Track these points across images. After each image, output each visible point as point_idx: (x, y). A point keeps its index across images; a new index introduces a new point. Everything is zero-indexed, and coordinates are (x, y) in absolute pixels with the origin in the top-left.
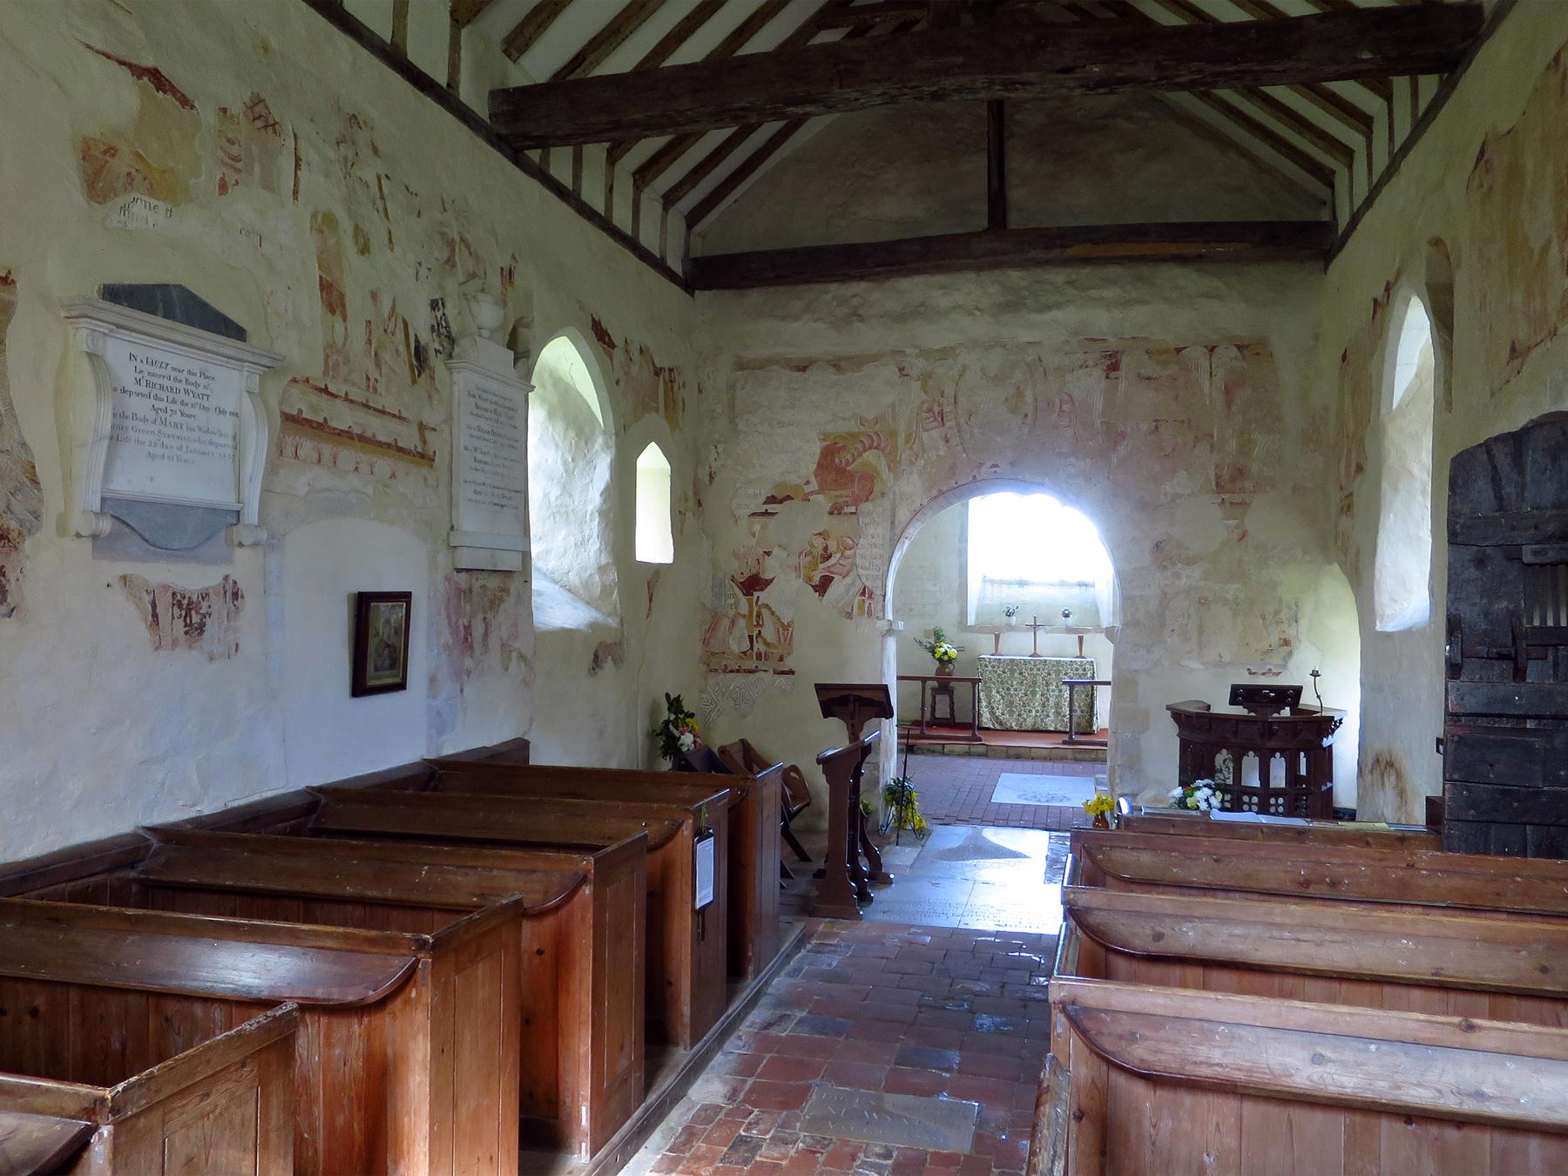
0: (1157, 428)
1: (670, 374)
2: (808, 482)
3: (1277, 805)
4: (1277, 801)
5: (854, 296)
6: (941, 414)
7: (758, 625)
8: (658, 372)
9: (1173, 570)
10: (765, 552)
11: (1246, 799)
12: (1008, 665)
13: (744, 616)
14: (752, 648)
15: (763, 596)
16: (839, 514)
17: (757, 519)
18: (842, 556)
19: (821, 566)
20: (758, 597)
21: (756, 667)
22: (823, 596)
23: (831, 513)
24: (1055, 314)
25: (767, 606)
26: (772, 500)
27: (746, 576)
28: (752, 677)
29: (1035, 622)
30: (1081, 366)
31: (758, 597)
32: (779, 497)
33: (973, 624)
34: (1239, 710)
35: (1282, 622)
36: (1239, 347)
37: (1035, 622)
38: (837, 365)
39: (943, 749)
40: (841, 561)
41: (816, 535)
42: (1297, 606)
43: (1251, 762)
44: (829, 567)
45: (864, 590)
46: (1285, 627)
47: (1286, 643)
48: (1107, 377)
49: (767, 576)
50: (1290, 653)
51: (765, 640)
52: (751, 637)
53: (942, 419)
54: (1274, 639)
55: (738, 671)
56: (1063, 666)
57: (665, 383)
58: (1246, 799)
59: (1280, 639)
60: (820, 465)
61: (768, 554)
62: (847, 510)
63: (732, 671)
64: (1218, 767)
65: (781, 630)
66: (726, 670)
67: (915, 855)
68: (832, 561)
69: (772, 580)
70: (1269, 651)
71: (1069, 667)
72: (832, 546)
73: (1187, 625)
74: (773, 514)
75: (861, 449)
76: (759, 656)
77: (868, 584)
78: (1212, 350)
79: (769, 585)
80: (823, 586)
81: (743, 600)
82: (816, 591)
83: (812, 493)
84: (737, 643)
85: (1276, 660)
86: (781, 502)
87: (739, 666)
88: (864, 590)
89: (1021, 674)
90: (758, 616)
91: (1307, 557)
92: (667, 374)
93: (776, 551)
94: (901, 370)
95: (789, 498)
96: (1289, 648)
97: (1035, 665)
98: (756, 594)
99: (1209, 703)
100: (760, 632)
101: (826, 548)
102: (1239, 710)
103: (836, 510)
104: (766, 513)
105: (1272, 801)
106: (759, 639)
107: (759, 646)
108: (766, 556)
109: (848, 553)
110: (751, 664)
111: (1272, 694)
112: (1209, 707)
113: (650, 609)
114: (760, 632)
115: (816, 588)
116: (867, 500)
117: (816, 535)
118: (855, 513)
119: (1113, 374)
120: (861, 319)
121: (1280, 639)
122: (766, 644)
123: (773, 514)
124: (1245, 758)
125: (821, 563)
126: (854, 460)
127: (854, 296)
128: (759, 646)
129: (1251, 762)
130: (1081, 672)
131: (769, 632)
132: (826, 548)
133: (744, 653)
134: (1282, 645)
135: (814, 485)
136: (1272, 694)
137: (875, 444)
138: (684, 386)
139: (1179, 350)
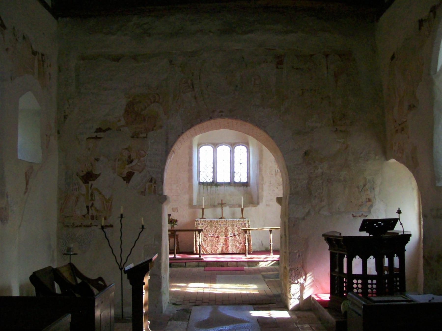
0: (303, 93)
1: (42, 58)
2: (119, 120)
3: (372, 284)
4: (370, 284)
5: (145, 24)
6: (193, 84)
7: (92, 200)
8: (34, 53)
9: (314, 165)
10: (96, 159)
11: (355, 281)
12: (209, 223)
13: (84, 195)
14: (88, 213)
15: (95, 184)
16: (138, 137)
17: (91, 140)
18: (139, 161)
19: (127, 166)
20: (92, 185)
21: (91, 224)
22: (129, 183)
23: (133, 137)
24: (250, 36)
25: (97, 189)
26: (99, 130)
27: (85, 172)
28: (89, 229)
29: (222, 202)
30: (264, 62)
31: (92, 185)
32: (104, 128)
33: (195, 205)
34: (365, 234)
35: (367, 190)
36: (340, 56)
37: (222, 202)
38: (135, 58)
39: (185, 265)
40: (139, 164)
41: (124, 149)
42: (373, 181)
43: (357, 262)
44: (131, 167)
45: (152, 179)
46: (369, 192)
47: (369, 200)
48: (277, 68)
49: (96, 172)
50: (372, 206)
51: (96, 208)
52: (87, 207)
53: (193, 87)
54: (364, 199)
55: (80, 226)
56: (235, 222)
57: (38, 60)
58: (369, 281)
59: (367, 198)
60: (126, 111)
61: (97, 160)
62: (142, 135)
63: (77, 226)
64: (126, 275)
65: (105, 202)
66: (74, 226)
67: (186, 326)
68: (133, 164)
69: (99, 175)
70: (361, 205)
71: (238, 223)
72: (133, 156)
73: (322, 193)
74: (100, 138)
75: (152, 101)
76: (92, 218)
77: (154, 176)
78: (327, 56)
79: (98, 177)
80: (128, 177)
81: (84, 186)
82: (124, 180)
83: (123, 126)
84: (80, 211)
85: (365, 209)
86: (104, 131)
87: (81, 224)
88: (152, 179)
89: (215, 227)
90: (92, 195)
91: (377, 157)
92: (40, 56)
93: (102, 158)
94: (171, 62)
95: (109, 129)
96: (371, 203)
97: (222, 223)
98: (90, 183)
99: (341, 232)
100: (93, 204)
101: (130, 157)
102: (365, 234)
103: (135, 136)
104: (96, 138)
105: (355, 281)
106: (92, 208)
107: (92, 212)
108: (96, 162)
109: (142, 159)
110: (88, 222)
111: (382, 224)
112: (341, 234)
113: (27, 189)
114: (93, 204)
115: (124, 179)
116: (153, 130)
117: (124, 149)
118: (146, 137)
119: (280, 66)
120: (149, 35)
121: (367, 198)
122: (97, 211)
123: (100, 138)
124: (368, 259)
125: (127, 165)
126: (145, 108)
127: (145, 24)
128: (92, 212)
129: (357, 262)
130: (243, 225)
131: (98, 204)
132: (130, 157)
133: (84, 216)
134: (368, 202)
135: (123, 122)
136: (382, 224)
137: (157, 100)
138: (50, 66)
139: (311, 56)
